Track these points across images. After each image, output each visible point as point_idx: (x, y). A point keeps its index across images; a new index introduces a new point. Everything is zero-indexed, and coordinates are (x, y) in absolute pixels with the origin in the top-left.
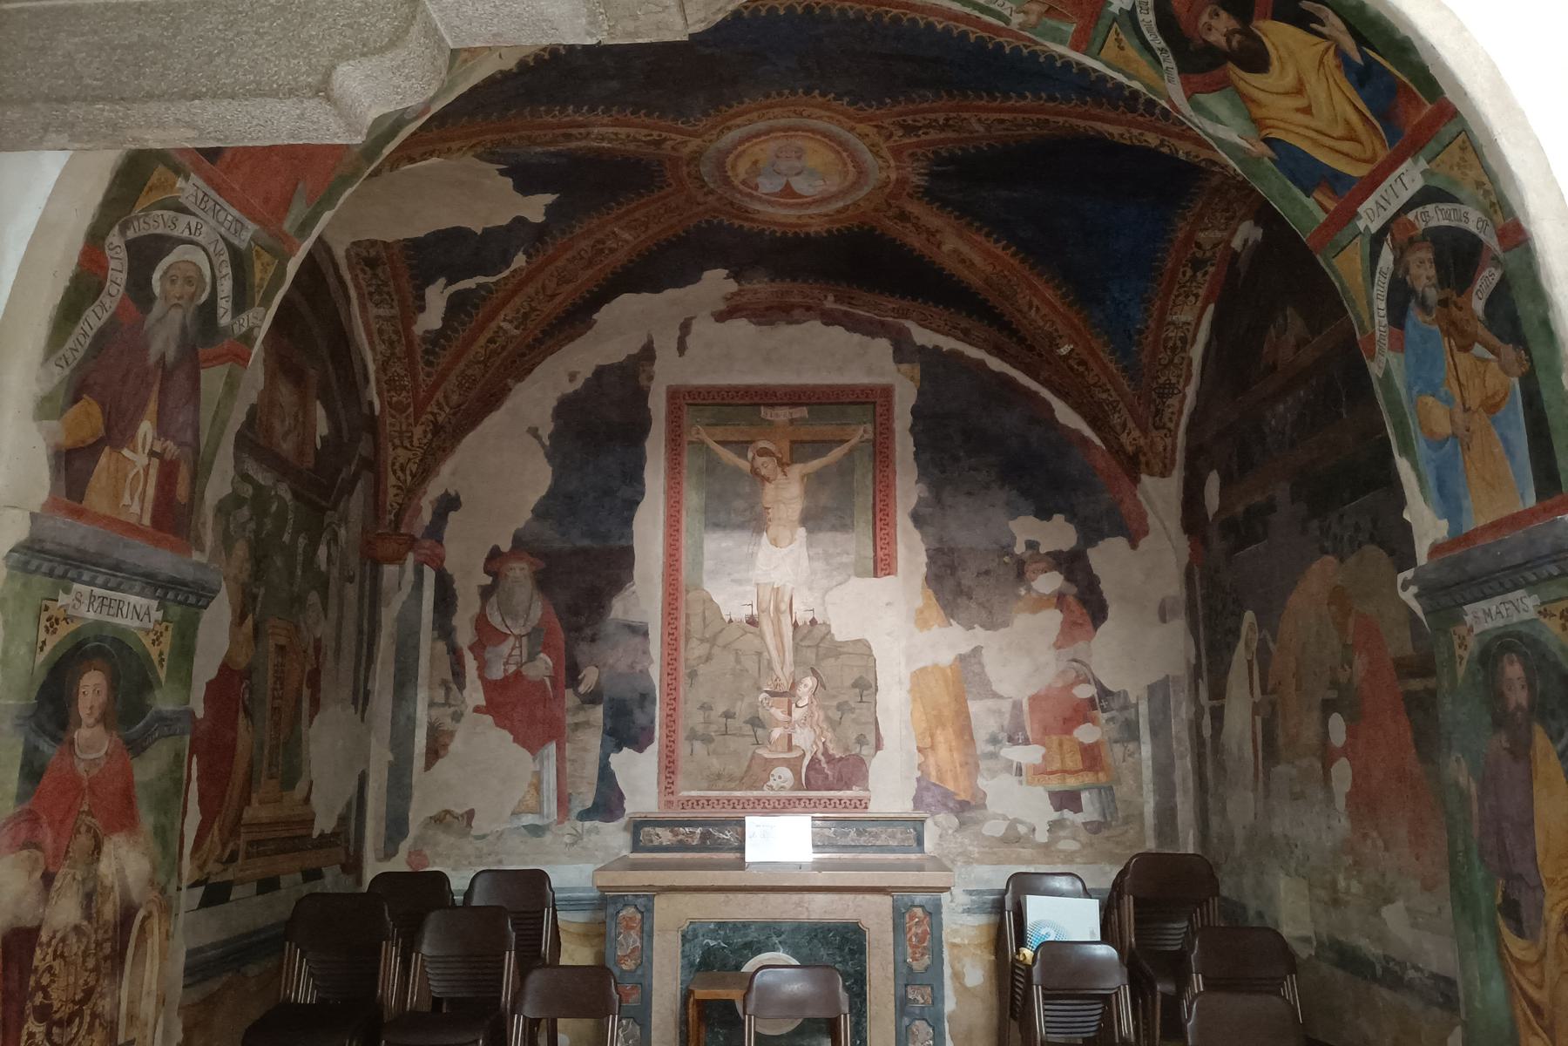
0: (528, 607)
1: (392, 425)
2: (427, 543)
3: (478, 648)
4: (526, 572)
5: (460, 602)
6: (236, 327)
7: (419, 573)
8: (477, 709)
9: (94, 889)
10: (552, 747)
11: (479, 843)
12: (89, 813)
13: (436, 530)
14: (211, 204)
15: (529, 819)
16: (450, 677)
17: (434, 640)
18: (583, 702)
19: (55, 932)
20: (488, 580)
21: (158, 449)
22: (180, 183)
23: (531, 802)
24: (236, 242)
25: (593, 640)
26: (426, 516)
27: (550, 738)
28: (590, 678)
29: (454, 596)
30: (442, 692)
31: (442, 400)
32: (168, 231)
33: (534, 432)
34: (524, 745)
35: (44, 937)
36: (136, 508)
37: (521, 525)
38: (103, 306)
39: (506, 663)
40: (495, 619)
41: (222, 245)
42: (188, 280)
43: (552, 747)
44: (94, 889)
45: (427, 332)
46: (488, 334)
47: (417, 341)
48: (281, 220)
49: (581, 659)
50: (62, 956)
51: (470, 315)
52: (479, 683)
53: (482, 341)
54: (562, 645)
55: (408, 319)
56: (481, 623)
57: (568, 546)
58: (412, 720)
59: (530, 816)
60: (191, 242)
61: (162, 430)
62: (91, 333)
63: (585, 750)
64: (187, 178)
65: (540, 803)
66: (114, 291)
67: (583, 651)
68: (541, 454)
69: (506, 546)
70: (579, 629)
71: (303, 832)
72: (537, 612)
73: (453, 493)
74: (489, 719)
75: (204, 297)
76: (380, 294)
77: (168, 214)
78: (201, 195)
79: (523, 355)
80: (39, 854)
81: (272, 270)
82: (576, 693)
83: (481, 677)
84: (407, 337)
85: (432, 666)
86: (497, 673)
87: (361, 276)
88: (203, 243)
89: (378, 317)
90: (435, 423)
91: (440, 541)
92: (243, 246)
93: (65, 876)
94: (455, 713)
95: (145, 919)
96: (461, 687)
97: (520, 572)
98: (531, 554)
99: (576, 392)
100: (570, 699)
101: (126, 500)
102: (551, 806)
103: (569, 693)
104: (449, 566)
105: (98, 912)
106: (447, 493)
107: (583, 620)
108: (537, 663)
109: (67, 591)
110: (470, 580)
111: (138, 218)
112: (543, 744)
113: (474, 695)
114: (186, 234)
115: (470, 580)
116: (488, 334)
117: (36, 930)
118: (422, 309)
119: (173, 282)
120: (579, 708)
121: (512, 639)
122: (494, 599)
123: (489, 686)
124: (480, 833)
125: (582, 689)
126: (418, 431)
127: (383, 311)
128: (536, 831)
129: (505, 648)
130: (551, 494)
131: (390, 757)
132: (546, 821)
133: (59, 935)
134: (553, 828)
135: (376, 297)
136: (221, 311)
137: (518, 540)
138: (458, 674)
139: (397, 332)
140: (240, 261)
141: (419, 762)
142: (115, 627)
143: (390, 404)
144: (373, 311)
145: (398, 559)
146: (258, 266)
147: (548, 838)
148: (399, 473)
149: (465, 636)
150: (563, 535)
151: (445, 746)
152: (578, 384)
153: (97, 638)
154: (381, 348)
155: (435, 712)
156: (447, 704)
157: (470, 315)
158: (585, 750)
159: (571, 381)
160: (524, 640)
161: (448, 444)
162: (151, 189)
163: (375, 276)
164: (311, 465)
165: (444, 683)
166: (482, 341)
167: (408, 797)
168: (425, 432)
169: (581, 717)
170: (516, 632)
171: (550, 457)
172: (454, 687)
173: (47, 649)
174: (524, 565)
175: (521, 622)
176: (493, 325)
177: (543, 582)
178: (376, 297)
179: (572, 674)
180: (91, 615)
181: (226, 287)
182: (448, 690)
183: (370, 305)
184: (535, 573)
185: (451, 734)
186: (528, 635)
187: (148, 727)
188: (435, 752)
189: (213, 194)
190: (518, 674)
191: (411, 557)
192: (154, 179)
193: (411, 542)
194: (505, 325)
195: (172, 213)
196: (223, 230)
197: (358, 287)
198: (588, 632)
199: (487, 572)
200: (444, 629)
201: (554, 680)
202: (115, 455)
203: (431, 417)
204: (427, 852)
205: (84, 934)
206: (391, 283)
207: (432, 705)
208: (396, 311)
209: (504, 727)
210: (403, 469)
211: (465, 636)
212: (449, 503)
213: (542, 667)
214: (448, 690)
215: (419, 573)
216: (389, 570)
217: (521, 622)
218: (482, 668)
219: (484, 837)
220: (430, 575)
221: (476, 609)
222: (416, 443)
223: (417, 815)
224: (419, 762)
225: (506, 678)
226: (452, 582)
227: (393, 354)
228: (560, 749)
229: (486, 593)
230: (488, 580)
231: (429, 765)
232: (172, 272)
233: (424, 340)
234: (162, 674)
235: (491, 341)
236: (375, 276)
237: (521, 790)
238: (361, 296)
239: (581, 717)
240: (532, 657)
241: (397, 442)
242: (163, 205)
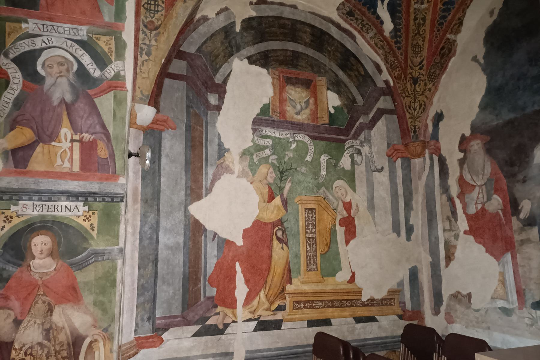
0: (484, 166)
1: (399, 87)
2: (432, 143)
3: (461, 195)
4: (480, 145)
5: (450, 172)
6: (106, 74)
7: (431, 159)
8: (465, 232)
9: (51, 328)
10: (508, 256)
11: (477, 314)
12: (44, 295)
13: (435, 136)
14: (50, 28)
15: (501, 303)
16: (450, 215)
17: (441, 194)
18: (524, 226)
19: (24, 345)
20: (461, 155)
21: (76, 137)
22: (24, 25)
23: (501, 292)
24: (79, 38)
25: (524, 181)
26: (430, 128)
27: (507, 250)
28: (526, 207)
29: (447, 168)
30: (448, 223)
31: (411, 65)
32: (32, 48)
33: (475, 59)
34: (492, 254)
35: (16, 345)
36: (67, 165)
37: (474, 117)
38: (13, 89)
39: (476, 204)
40: (468, 177)
41: (70, 43)
42: (61, 64)
43: (508, 256)
44: (51, 328)
45: (390, 33)
46: (412, 17)
47: (389, 39)
48: (102, 17)
49: (518, 195)
50: (31, 354)
51: (400, 12)
52: (464, 216)
53: (412, 22)
54: (506, 188)
55: (380, 32)
56: (461, 181)
57: (500, 121)
58: (437, 239)
59: (502, 301)
60: (50, 47)
61: (75, 129)
62: (11, 101)
63: (530, 259)
64: (27, 22)
65: (506, 293)
66: (16, 81)
67: (519, 189)
68: (479, 69)
69: (468, 133)
70: (514, 175)
71: (358, 297)
72: (488, 169)
73: (439, 111)
74: (471, 238)
75: (75, 67)
76: (364, 26)
77: (26, 41)
78: (41, 27)
79: (444, 17)
80: (10, 312)
81: (113, 42)
82: (518, 219)
83: (465, 213)
84: (386, 42)
85: (442, 208)
86: (472, 210)
87: (351, 22)
88: (57, 45)
89: (371, 38)
90: (413, 78)
91: (437, 140)
92: (85, 38)
93: (29, 321)
94: (455, 234)
95: (91, 343)
96: (456, 220)
97: (476, 145)
98: (482, 134)
99: (495, 22)
100: (515, 223)
101: (59, 162)
102: (514, 297)
103: (514, 219)
104: (444, 153)
105: (55, 337)
106: (437, 113)
107: (516, 168)
108: (493, 201)
109: (16, 205)
110: (453, 156)
111: (11, 48)
112: (503, 254)
113: (463, 224)
114: (44, 45)
115: (453, 156)
116: (412, 17)
117: (12, 343)
118: (382, 23)
119: (51, 67)
120: (522, 230)
121: (477, 188)
122: (465, 166)
123: (470, 218)
124: (476, 308)
125: (522, 216)
126: (408, 85)
127: (371, 34)
128: (506, 312)
129: (475, 194)
130: (489, 91)
131: (430, 259)
132: (511, 307)
133: (27, 346)
134: (517, 311)
135: (364, 29)
136: (91, 71)
137: (474, 128)
138: (454, 213)
139: (381, 41)
140: (86, 45)
141: (443, 263)
142: (54, 216)
143: (395, 77)
144: (368, 36)
145: (421, 155)
146: (101, 44)
147: (514, 318)
148: (410, 111)
149: (454, 190)
150: (497, 116)
151: (453, 254)
152: (495, 17)
153: (40, 222)
154: (381, 52)
155: (447, 234)
156: (451, 230)
157: (400, 12)
158: (530, 259)
159: (491, 16)
160: (484, 187)
161: (430, 86)
162: (9, 34)
163: (357, 19)
164: (327, 121)
165: (448, 218)
166: (412, 22)
167: (440, 282)
168: (411, 84)
169: (524, 236)
170: (479, 184)
171: (484, 70)
172: (453, 220)
173: (5, 230)
174: (479, 141)
175: (481, 176)
176: (412, 10)
177: (489, 150)
178: (364, 29)
179: (513, 206)
180: (36, 213)
181: (86, 60)
182: (450, 221)
183: (365, 34)
184: (485, 144)
185: (455, 247)
186: (485, 184)
187: (88, 256)
188: (449, 258)
189: (48, 23)
190: (483, 209)
191: (427, 152)
192: (8, 30)
193: (425, 144)
194: (417, 6)
195: (30, 40)
196: (66, 36)
197: (356, 29)
198: (520, 177)
199: (461, 150)
200: (445, 189)
201: (504, 210)
202: (46, 146)
203: (410, 76)
204: (452, 314)
205: (46, 347)
206: (364, 19)
207: (444, 230)
208: (375, 31)
209: (480, 243)
210: (409, 107)
211: (454, 190)
212: (439, 117)
213: (496, 203)
214: (450, 221)
215: (431, 159)
216: (417, 162)
217: (481, 176)
218: (464, 208)
219: (478, 310)
220: (436, 158)
221: (458, 174)
222: (410, 93)
223: (446, 293)
224: (443, 263)
225: (477, 212)
226: (446, 160)
227: (386, 52)
228: (514, 257)
229: (462, 162)
230: (461, 155)
231: (447, 265)
232: (47, 63)
233: (392, 37)
234: (94, 234)
235: (415, 19)
236: (357, 19)
237: (494, 284)
238: (359, 32)
239: (524, 236)
240: (489, 199)
241: (404, 95)
242: (21, 38)
